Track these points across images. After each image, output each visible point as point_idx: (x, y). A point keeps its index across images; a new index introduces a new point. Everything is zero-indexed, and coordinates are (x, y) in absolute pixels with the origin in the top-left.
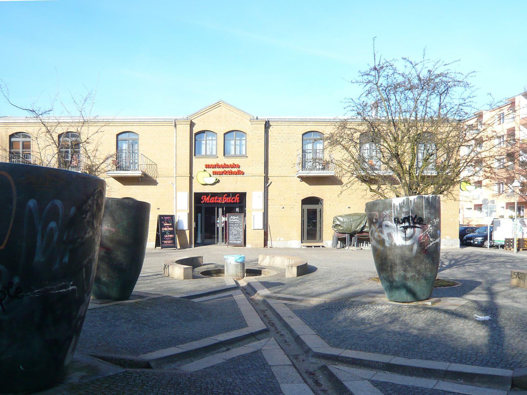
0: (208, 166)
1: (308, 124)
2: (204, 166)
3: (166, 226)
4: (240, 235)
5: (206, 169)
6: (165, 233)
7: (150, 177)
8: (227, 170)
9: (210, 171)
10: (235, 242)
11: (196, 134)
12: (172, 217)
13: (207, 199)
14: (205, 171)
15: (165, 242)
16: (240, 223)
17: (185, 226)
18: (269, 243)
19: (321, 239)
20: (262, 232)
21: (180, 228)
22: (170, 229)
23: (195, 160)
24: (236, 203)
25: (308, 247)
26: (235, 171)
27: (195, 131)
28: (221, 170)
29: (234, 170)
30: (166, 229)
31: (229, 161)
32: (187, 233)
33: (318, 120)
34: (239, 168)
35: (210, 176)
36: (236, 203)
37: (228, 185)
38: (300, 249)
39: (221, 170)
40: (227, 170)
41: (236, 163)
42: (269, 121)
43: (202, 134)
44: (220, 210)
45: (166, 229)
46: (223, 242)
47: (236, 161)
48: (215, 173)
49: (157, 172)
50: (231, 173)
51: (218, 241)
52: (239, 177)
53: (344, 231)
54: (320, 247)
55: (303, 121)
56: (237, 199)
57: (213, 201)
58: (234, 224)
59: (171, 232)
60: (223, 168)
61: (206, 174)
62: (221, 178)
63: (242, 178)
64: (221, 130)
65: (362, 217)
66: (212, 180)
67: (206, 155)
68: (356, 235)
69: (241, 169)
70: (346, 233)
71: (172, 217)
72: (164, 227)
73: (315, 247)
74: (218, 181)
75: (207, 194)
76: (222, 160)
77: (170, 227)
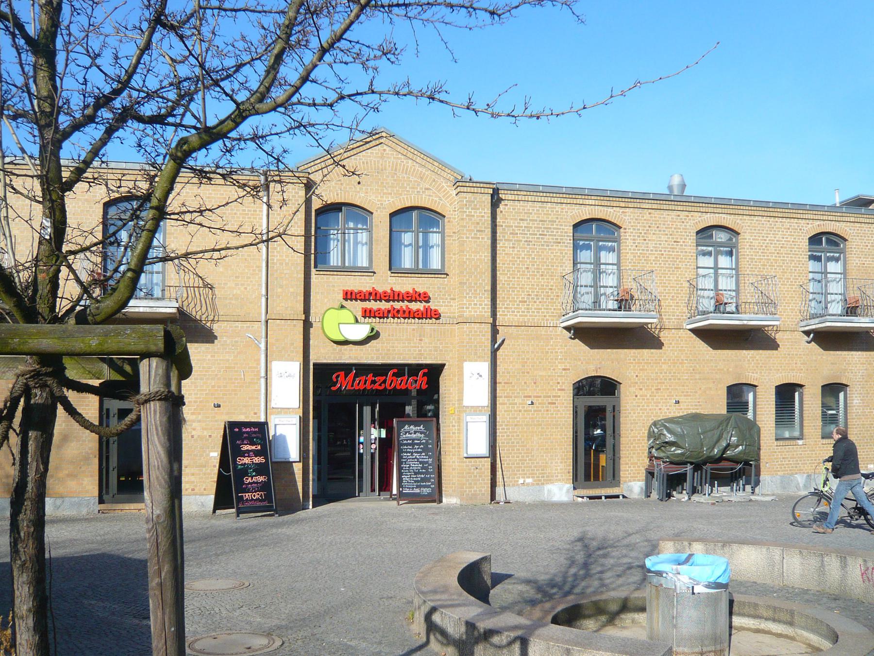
0: (349, 296)
1: (587, 202)
2: (341, 296)
3: (248, 451)
4: (427, 473)
5: (344, 303)
6: (244, 472)
7: (196, 321)
8: (397, 305)
9: (359, 306)
10: (417, 491)
11: (319, 212)
12: (262, 427)
13: (343, 383)
14: (342, 307)
15: (247, 496)
16: (427, 443)
17: (293, 453)
18: (499, 490)
19: (614, 478)
20: (487, 463)
21: (278, 457)
22: (258, 460)
23: (315, 278)
24: (415, 393)
25: (591, 498)
26: (416, 308)
27: (316, 204)
28: (384, 305)
29: (415, 306)
30: (246, 460)
31: (404, 285)
32: (298, 468)
33: (713, 201)
34: (428, 301)
35: (357, 321)
36: (415, 393)
37: (402, 344)
38: (572, 505)
39: (384, 305)
40: (397, 305)
41: (420, 290)
42: (498, 189)
43: (331, 215)
44: (367, 410)
45: (246, 460)
46: (373, 490)
47: (419, 284)
48: (368, 314)
49: (214, 309)
50: (409, 315)
51: (361, 490)
52: (428, 325)
53: (684, 459)
54: (600, 497)
55: (575, 194)
56: (421, 381)
57: (361, 387)
58: (413, 444)
59: (261, 469)
60: (388, 301)
61: (346, 315)
62: (389, 327)
63: (436, 327)
64: (381, 202)
65: (721, 423)
66: (361, 331)
67: (344, 266)
68: (708, 466)
69: (432, 305)
70: (685, 463)
71: (262, 427)
72: (243, 454)
73: (606, 497)
74: (374, 336)
75: (346, 368)
76: (385, 281)
77: (257, 453)
